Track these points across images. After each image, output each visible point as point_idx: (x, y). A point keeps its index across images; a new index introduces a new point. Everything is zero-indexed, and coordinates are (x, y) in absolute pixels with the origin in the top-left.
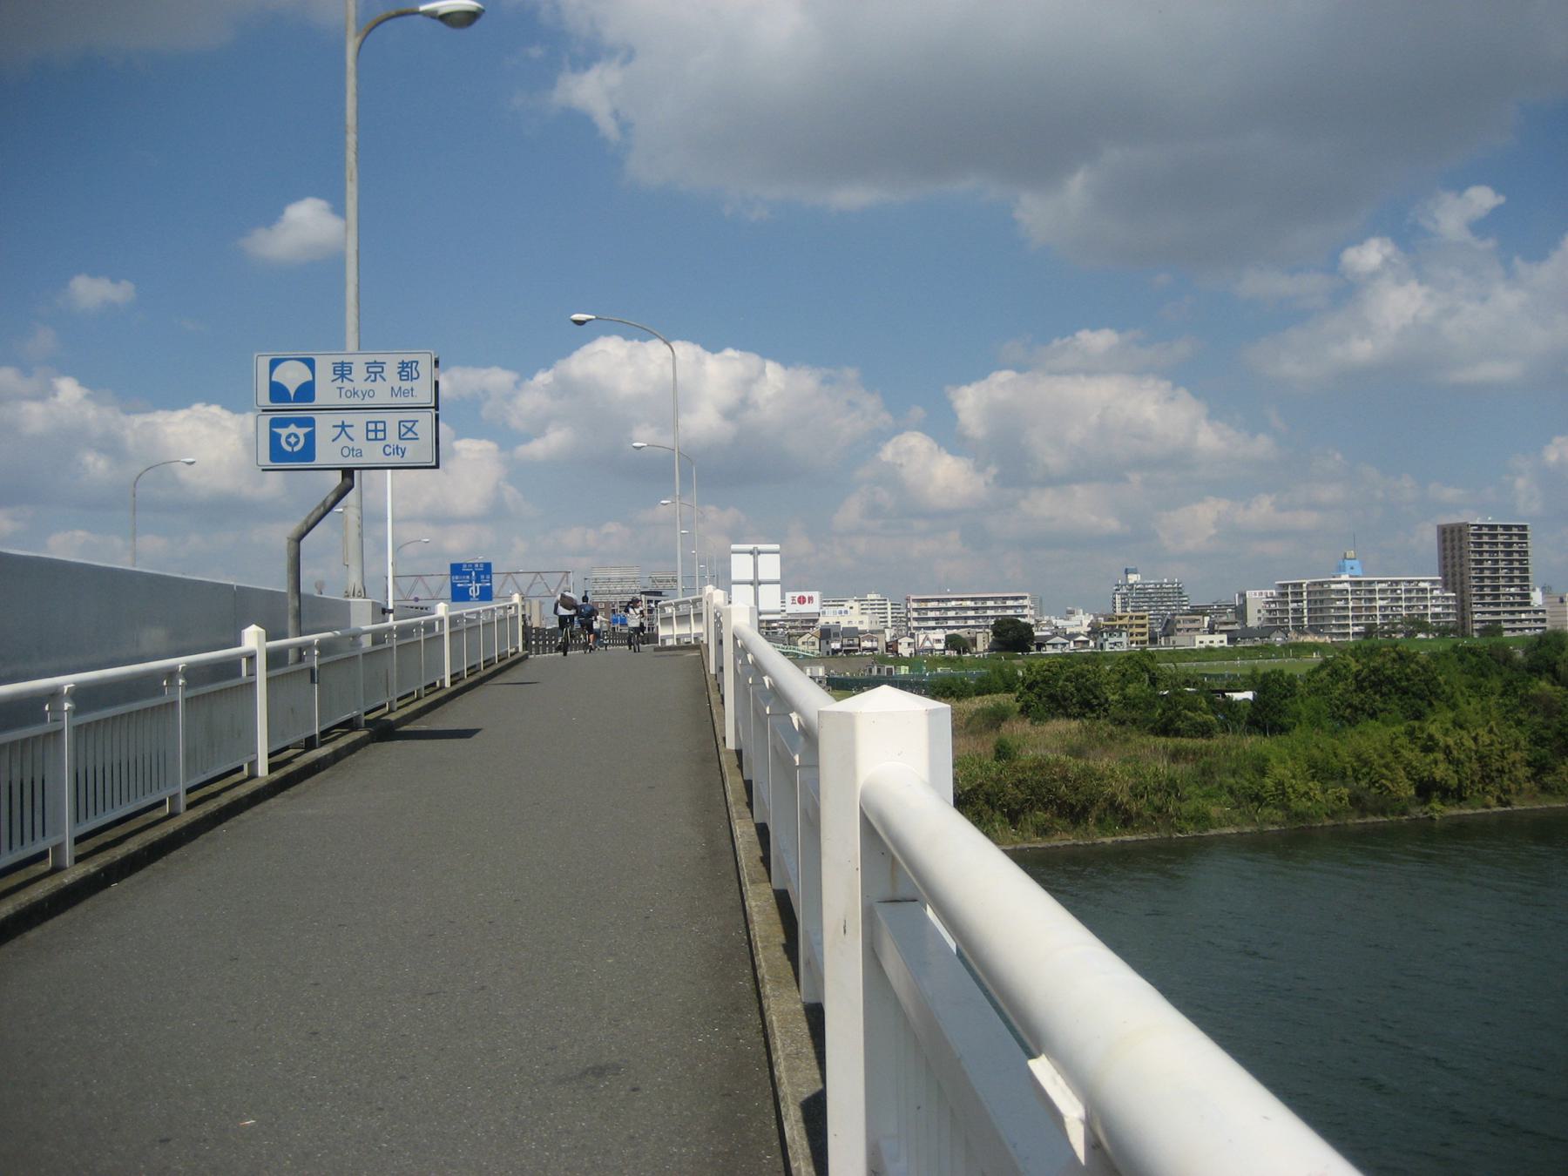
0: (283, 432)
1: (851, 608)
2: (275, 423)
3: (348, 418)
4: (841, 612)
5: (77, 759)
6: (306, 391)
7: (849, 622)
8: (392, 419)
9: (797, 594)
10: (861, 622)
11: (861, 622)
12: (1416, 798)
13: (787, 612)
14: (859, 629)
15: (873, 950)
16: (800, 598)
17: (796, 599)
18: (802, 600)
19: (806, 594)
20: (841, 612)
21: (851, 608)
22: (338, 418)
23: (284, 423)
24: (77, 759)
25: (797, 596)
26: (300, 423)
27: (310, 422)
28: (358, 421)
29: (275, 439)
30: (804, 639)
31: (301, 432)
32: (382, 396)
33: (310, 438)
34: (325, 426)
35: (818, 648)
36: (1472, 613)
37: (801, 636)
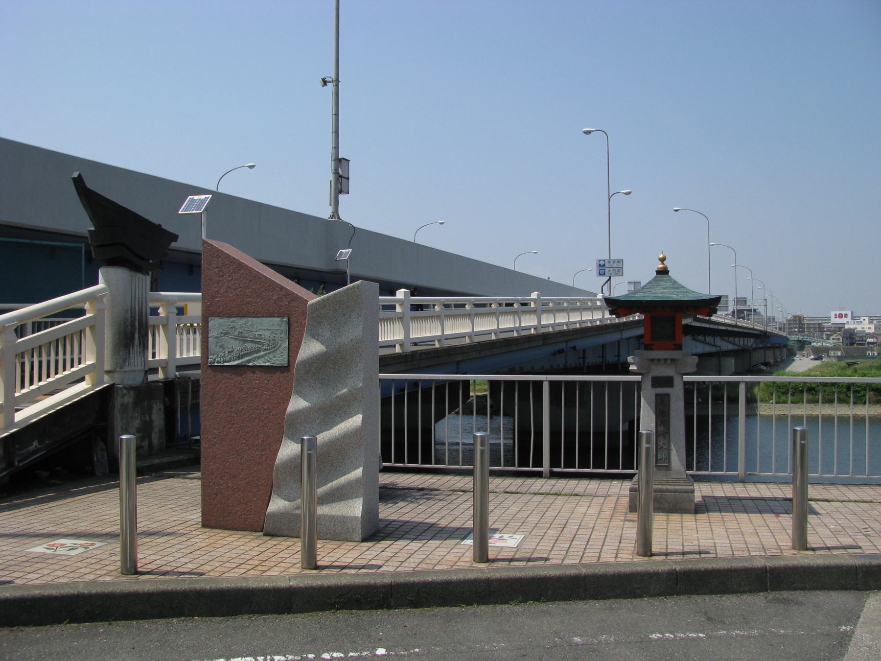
0: (600, 271)
1: (864, 320)
2: (600, 270)
3: (610, 269)
4: (858, 322)
5: (428, 367)
6: (604, 265)
7: (862, 328)
8: (616, 269)
9: (838, 313)
10: (869, 328)
11: (869, 328)
12: (641, 472)
13: (832, 322)
14: (866, 331)
15: (169, 534)
16: (839, 314)
17: (837, 315)
18: (841, 316)
19: (843, 313)
20: (858, 322)
21: (864, 320)
22: (609, 269)
23: (601, 270)
24: (428, 367)
25: (838, 314)
26: (603, 270)
27: (604, 270)
28: (611, 269)
29: (600, 272)
30: (834, 336)
31: (603, 271)
32: (615, 266)
33: (605, 272)
34: (607, 270)
35: (841, 341)
36: (744, 345)
37: (832, 335)
